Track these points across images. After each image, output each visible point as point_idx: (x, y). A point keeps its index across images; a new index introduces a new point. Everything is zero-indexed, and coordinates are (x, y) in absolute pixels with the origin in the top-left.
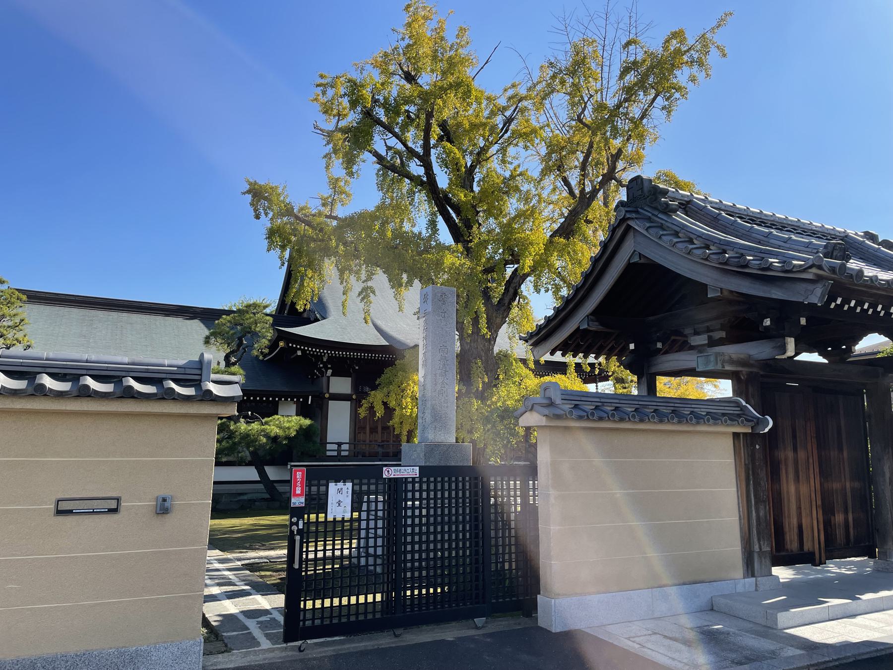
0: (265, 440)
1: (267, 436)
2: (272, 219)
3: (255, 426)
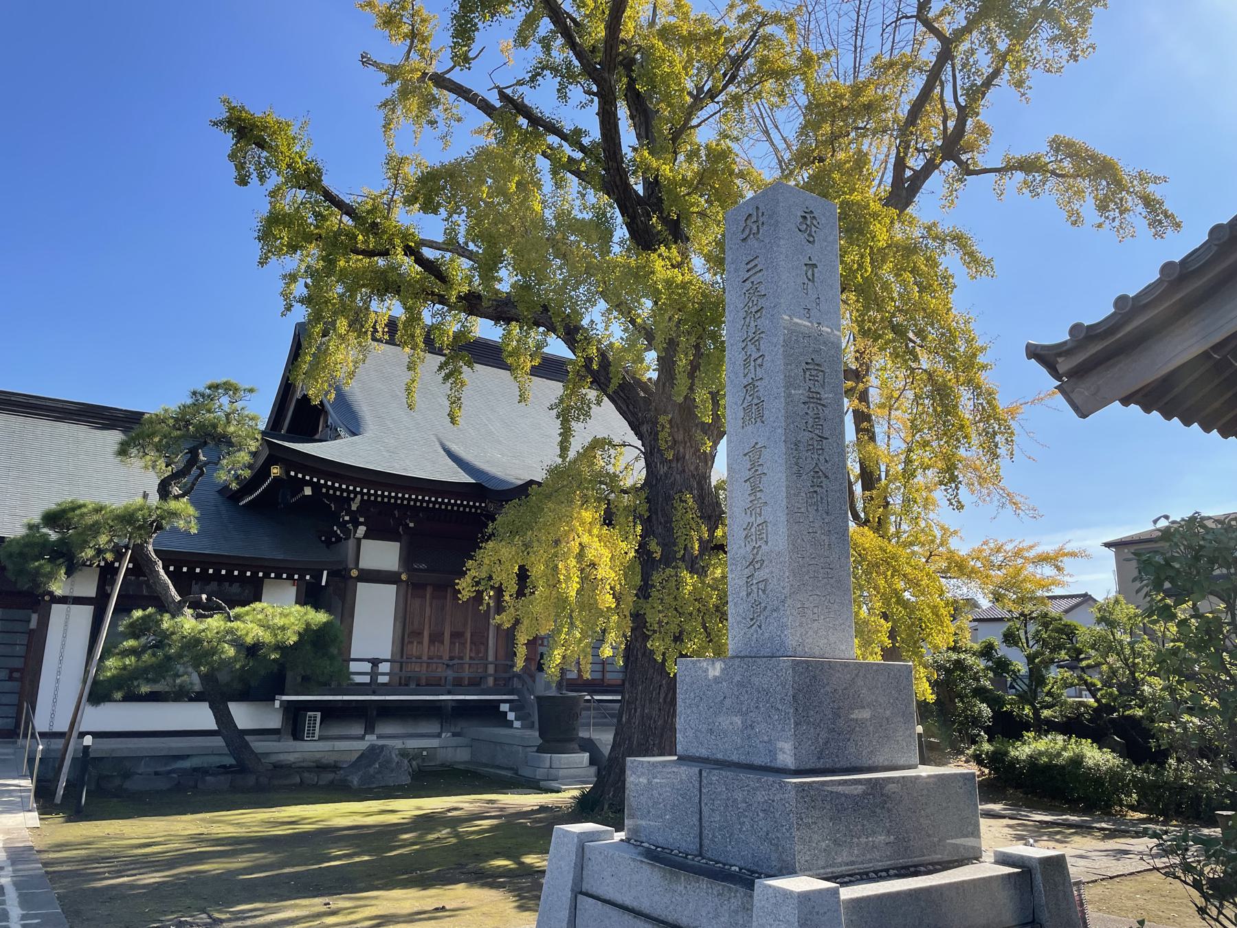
0: (231, 652)
1: (238, 643)
2: (273, 194)
3: (215, 623)
